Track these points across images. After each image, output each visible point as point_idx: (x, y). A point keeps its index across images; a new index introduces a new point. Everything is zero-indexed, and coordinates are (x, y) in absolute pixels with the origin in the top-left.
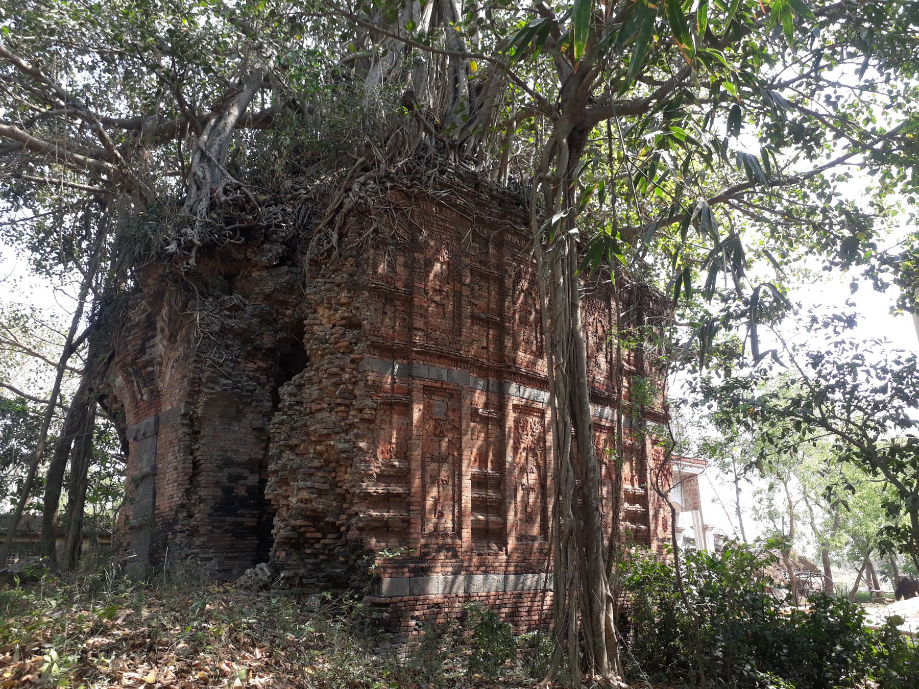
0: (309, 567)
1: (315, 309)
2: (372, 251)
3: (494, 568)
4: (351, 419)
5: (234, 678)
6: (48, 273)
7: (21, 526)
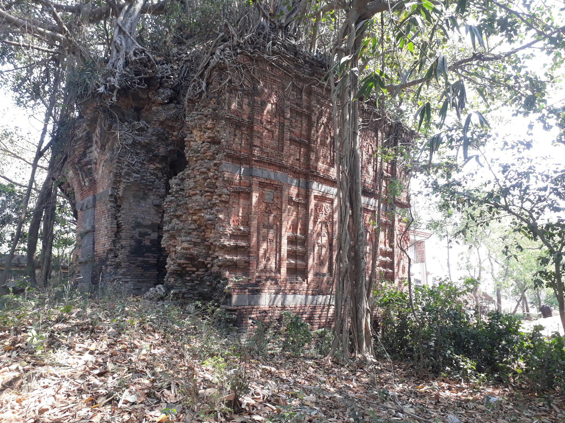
2: (228, 94)
3: (300, 291)
5: (142, 349)
6: (25, 106)
7: (14, 261)
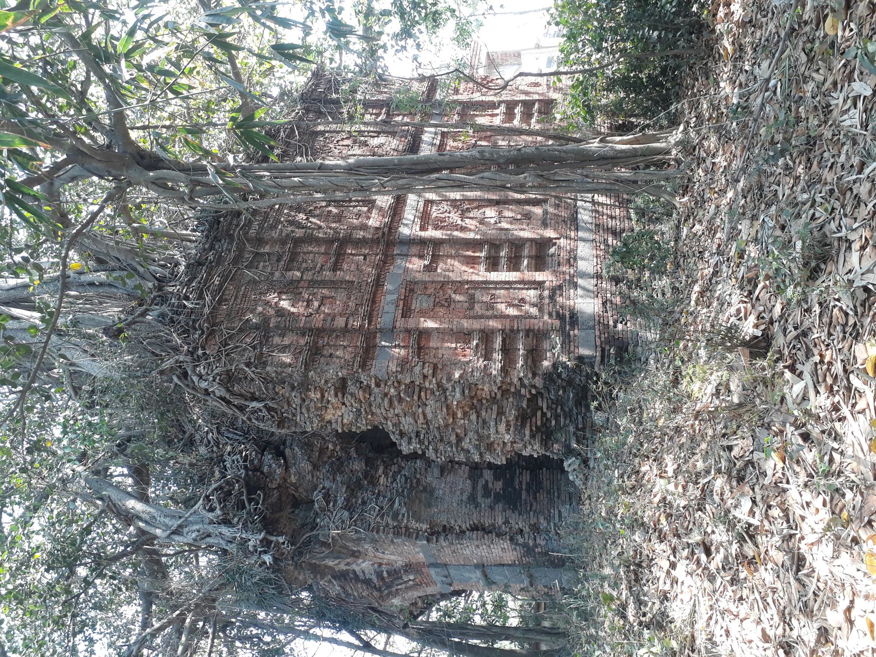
0: (567, 422)
1: (327, 422)
2: (268, 368)
4: (433, 386)
